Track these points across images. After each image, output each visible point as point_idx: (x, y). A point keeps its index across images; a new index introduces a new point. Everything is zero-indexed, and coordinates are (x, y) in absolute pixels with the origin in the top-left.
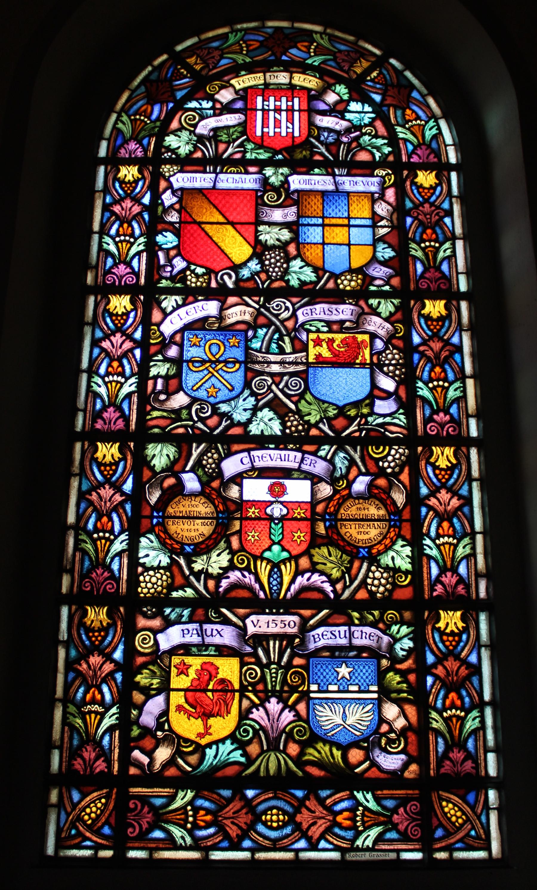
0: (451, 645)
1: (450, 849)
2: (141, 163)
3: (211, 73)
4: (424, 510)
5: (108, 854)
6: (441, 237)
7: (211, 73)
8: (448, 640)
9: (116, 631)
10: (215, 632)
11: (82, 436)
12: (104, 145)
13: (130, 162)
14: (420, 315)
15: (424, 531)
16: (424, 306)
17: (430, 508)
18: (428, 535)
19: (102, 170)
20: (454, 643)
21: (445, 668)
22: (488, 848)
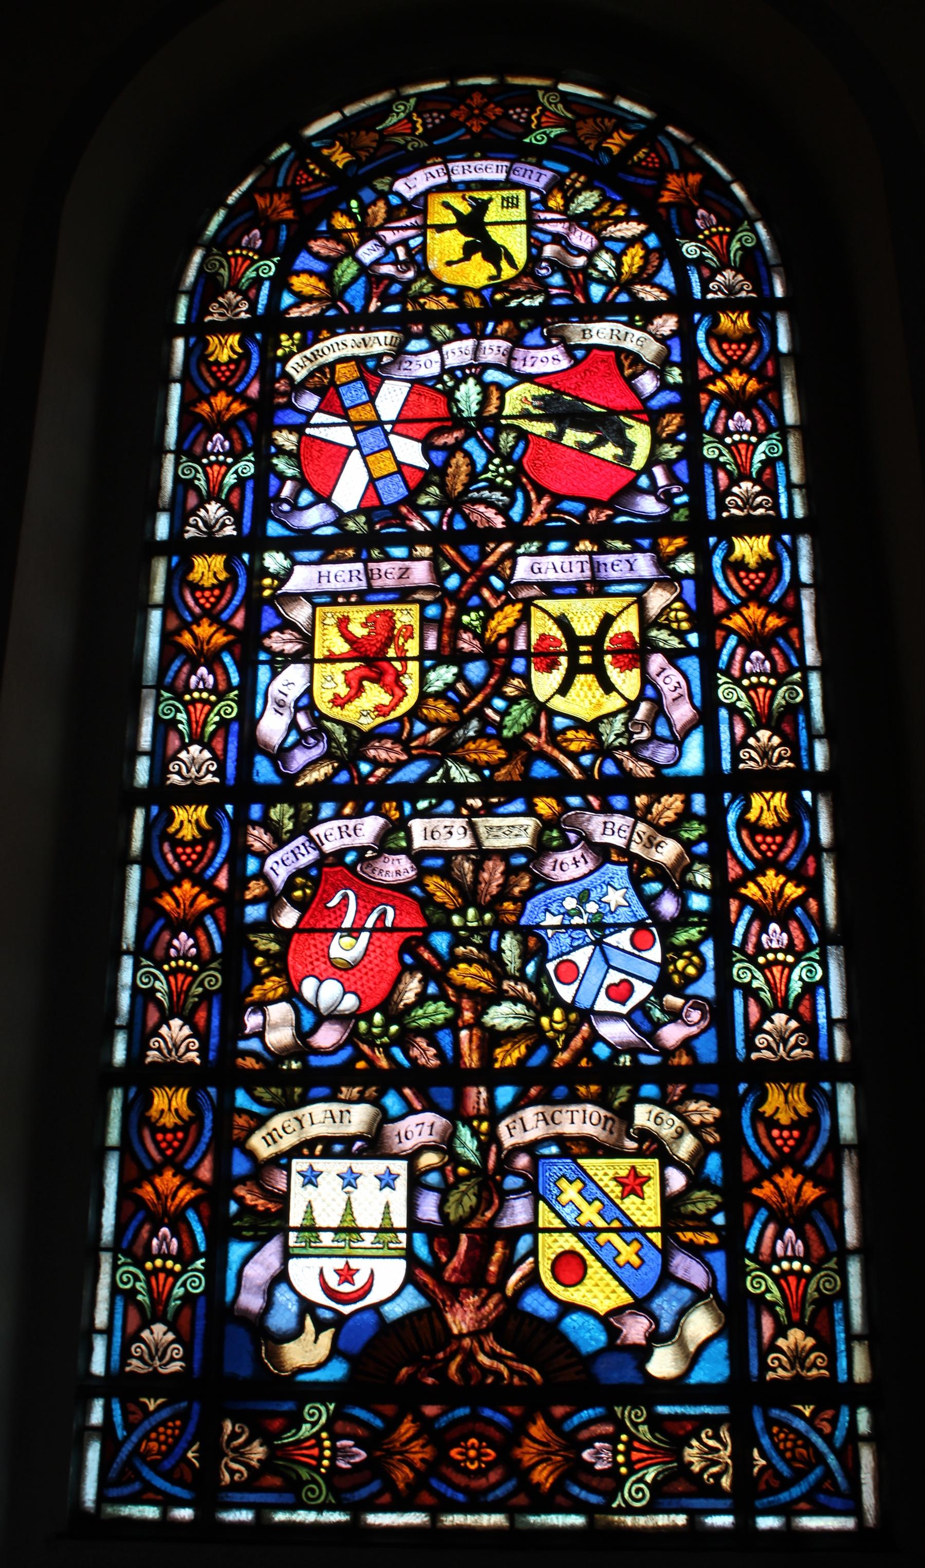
0: (769, 849)
1: (788, 1511)
2: (244, 329)
3: (361, 172)
4: (734, 905)
5: (185, 1514)
6: (761, 428)
7: (361, 172)
8: (764, 842)
9: (200, 1134)
10: (284, 690)
11: (144, 797)
12: (183, 305)
13: (224, 329)
14: (757, 1116)
15: (736, 944)
16: (762, 1098)
17: (745, 901)
18: (742, 949)
19: (180, 344)
20: (774, 847)
21: (760, 886)
22: (856, 1510)
